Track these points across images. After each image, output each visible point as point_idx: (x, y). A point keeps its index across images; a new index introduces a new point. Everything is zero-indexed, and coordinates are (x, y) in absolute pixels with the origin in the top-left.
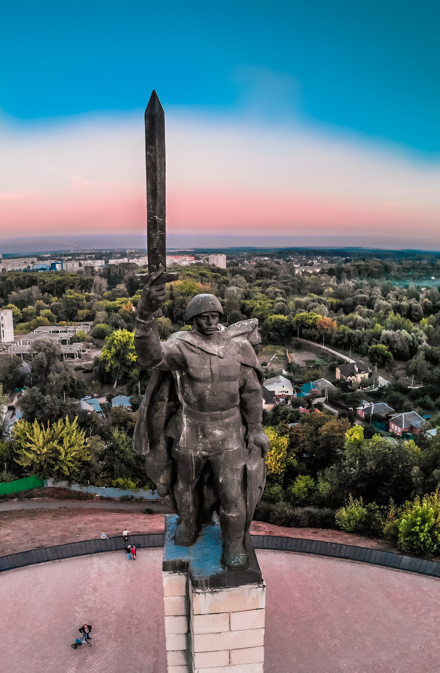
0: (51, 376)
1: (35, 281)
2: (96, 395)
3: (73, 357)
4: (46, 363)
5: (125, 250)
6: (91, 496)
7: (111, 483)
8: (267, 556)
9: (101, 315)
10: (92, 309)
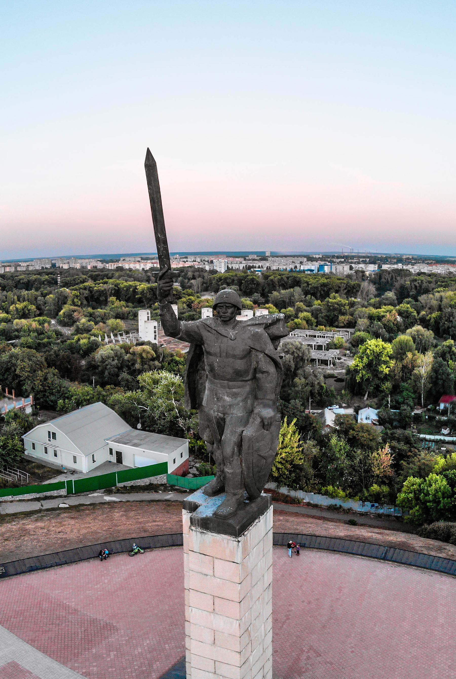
0: (297, 380)
1: (299, 282)
2: (344, 405)
3: (327, 364)
4: (293, 366)
5: (402, 255)
6: (298, 500)
7: (320, 490)
8: (431, 578)
9: (363, 322)
10: (354, 316)
